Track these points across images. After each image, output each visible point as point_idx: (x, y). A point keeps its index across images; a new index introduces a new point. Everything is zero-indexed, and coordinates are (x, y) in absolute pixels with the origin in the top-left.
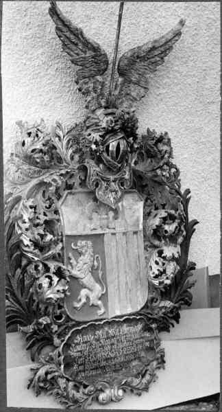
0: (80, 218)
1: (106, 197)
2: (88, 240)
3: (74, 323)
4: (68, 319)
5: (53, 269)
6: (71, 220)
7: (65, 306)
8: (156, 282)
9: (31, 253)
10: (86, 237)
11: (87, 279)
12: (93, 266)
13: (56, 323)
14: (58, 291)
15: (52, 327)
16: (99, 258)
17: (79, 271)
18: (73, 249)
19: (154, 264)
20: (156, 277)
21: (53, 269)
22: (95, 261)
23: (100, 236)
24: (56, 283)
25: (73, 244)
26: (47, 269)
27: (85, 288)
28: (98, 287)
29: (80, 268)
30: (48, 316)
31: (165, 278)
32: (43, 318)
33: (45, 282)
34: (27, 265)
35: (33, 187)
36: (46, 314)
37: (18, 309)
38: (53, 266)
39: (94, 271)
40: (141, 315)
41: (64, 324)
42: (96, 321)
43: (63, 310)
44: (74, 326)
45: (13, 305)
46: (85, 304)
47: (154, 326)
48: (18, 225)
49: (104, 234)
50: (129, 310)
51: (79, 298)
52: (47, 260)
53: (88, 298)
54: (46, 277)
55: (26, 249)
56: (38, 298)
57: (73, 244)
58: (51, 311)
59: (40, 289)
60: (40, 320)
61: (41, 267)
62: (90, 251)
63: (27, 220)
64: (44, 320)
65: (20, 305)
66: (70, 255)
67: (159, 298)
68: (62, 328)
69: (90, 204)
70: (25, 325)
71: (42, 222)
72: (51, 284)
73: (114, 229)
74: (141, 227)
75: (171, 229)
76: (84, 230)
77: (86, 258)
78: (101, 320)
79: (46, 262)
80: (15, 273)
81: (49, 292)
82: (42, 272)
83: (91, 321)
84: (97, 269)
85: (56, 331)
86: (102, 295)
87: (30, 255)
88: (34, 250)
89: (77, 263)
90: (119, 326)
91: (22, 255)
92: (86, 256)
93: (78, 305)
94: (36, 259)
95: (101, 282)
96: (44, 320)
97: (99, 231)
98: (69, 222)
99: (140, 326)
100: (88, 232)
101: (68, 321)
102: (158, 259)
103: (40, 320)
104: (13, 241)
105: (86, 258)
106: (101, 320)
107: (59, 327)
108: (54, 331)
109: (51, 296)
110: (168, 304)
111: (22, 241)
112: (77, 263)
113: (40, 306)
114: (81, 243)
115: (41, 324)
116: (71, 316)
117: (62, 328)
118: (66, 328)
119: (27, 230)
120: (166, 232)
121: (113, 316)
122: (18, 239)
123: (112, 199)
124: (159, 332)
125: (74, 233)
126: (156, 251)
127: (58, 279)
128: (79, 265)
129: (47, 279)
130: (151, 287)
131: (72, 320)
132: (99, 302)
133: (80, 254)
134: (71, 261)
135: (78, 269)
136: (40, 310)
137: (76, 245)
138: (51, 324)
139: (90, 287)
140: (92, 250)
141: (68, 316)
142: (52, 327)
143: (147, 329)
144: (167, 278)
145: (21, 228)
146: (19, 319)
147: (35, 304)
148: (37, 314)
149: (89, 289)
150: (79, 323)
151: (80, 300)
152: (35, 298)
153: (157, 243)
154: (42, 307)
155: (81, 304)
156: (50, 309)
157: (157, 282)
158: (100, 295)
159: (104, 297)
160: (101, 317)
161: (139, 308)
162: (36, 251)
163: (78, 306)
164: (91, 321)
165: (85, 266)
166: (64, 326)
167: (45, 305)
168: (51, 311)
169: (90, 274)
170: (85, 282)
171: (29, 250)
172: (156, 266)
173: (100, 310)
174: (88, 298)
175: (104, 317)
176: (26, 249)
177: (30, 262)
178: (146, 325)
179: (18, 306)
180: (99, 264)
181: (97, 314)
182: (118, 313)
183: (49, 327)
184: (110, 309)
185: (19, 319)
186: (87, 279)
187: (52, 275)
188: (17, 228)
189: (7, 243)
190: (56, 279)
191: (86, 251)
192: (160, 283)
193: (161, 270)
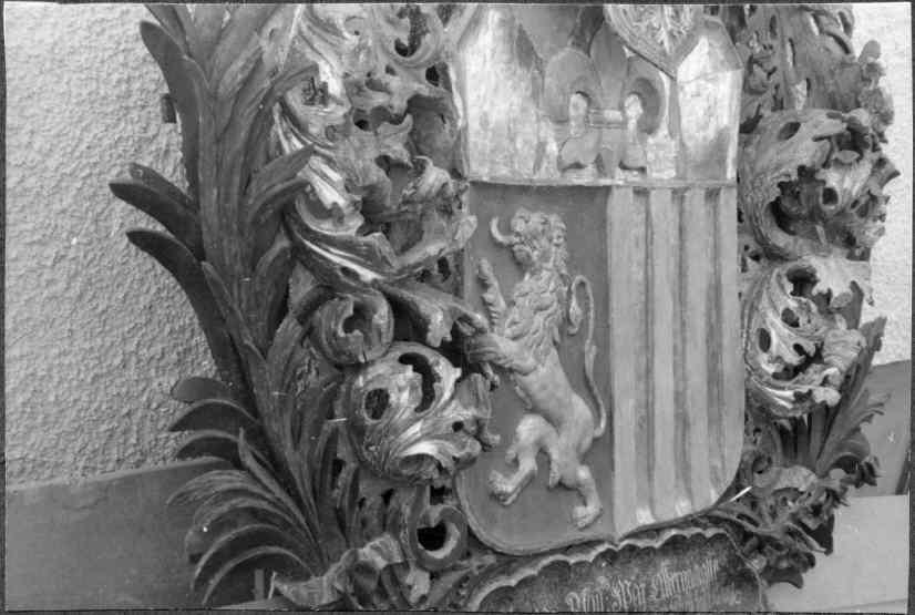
0: (524, 110)
1: (643, 25)
2: (550, 212)
3: (490, 559)
4: (473, 543)
5: (439, 327)
6: (494, 118)
7: (462, 491)
8: (783, 396)
9: (347, 246)
10: (546, 195)
11: (545, 375)
12: (567, 320)
13: (421, 565)
14: (458, 426)
15: (409, 580)
16: (589, 290)
17: (515, 338)
18: (499, 245)
19: (778, 322)
20: (791, 373)
21: (439, 327)
22: (574, 303)
23: (597, 196)
24: (447, 395)
25: (494, 223)
26: (409, 323)
27: (534, 410)
28: (580, 408)
29: (519, 328)
30: (395, 532)
31: (818, 378)
32: (377, 542)
33: (402, 388)
34: (313, 305)
35: (332, 168)
36: (390, 524)
37: (276, 503)
38: (437, 314)
39: (568, 342)
40: (717, 521)
41: (454, 569)
42: (568, 549)
43: (450, 504)
44: (488, 573)
45: (257, 489)
46: (531, 479)
47: (756, 565)
48: (287, 112)
49: (608, 189)
50: (682, 508)
51: (511, 453)
52: (402, 283)
53: (543, 454)
54: (405, 360)
55: (326, 228)
56: (356, 454)
57: (494, 223)
58: (407, 511)
59: (376, 415)
60: (367, 553)
61: (382, 315)
62: (558, 255)
63: (335, 87)
64: (377, 552)
65: (288, 485)
66: (486, 266)
67: (777, 457)
68: (449, 580)
69: (562, 55)
70: (299, 575)
71: (399, 104)
72: (428, 396)
73: (642, 170)
74: (731, 174)
75: (847, 184)
76: (537, 166)
77: (541, 286)
78: (589, 544)
79: (406, 294)
80: (271, 337)
81: (416, 428)
82: (388, 336)
83: (552, 552)
84: (579, 337)
85: (423, 598)
86: (596, 440)
87: (336, 257)
88: (363, 231)
89: (511, 303)
90: (644, 569)
91: (298, 255)
92: (545, 274)
93: (507, 485)
94: (368, 275)
95: (590, 389)
96: (377, 552)
97: (586, 178)
98: (484, 122)
99: (711, 567)
100: (548, 175)
101: (468, 555)
102: (792, 304)
103: (367, 553)
104: (269, 184)
105: (541, 286)
106: (589, 544)
107: (434, 576)
108: (413, 598)
109: (425, 448)
110: (800, 478)
111: (303, 188)
112: (511, 303)
113: (363, 487)
114: (528, 220)
115: (366, 569)
116: (483, 535)
117: (449, 580)
118: (459, 585)
119: (331, 132)
120: (830, 195)
121: (629, 528)
122: (284, 93)
123: (663, 36)
124: (770, 583)
125: (503, 173)
126: (781, 270)
127: (458, 373)
128: (515, 314)
129: (409, 372)
130: (759, 412)
131: (483, 548)
132: (584, 473)
133: (522, 266)
134: (489, 296)
135: (508, 332)
136: (362, 503)
137: (507, 229)
138: (405, 566)
139: (551, 406)
140: (562, 252)
141: (471, 535)
142: (409, 580)
143: (737, 577)
144: (825, 382)
145: (298, 126)
146: (274, 550)
147: (345, 477)
148: (344, 525)
149: (549, 418)
150: (508, 562)
151: (516, 462)
152: (343, 452)
153: (780, 239)
154: (370, 491)
155: (518, 478)
156: (404, 503)
157: (789, 394)
158: (587, 442)
159: (599, 452)
160: (588, 535)
161: (714, 497)
162: (376, 238)
163: (509, 488)
164: (552, 552)
165: (539, 319)
166: (455, 577)
167: (384, 486)
168: (407, 511)
169: (554, 351)
170: (535, 388)
171: (341, 233)
172: (786, 331)
173: (585, 504)
174: (543, 454)
175: (599, 531)
176: (326, 228)
177: (331, 285)
178: (736, 561)
179: (278, 492)
180: (587, 310)
181: (574, 521)
182: (645, 518)
183: (396, 582)
184: (618, 501)
185: (274, 550)
186: (545, 375)
187: (430, 356)
188: (279, 128)
189: (244, 193)
190: (448, 374)
191: (545, 257)
192: (800, 398)
193: (810, 348)
